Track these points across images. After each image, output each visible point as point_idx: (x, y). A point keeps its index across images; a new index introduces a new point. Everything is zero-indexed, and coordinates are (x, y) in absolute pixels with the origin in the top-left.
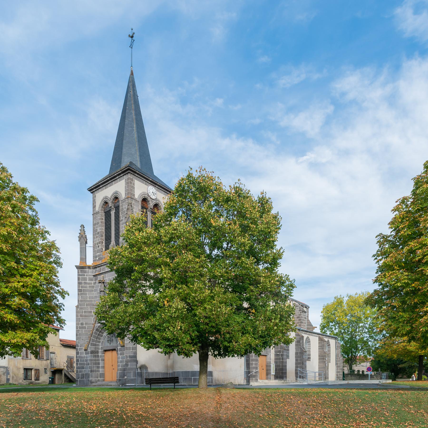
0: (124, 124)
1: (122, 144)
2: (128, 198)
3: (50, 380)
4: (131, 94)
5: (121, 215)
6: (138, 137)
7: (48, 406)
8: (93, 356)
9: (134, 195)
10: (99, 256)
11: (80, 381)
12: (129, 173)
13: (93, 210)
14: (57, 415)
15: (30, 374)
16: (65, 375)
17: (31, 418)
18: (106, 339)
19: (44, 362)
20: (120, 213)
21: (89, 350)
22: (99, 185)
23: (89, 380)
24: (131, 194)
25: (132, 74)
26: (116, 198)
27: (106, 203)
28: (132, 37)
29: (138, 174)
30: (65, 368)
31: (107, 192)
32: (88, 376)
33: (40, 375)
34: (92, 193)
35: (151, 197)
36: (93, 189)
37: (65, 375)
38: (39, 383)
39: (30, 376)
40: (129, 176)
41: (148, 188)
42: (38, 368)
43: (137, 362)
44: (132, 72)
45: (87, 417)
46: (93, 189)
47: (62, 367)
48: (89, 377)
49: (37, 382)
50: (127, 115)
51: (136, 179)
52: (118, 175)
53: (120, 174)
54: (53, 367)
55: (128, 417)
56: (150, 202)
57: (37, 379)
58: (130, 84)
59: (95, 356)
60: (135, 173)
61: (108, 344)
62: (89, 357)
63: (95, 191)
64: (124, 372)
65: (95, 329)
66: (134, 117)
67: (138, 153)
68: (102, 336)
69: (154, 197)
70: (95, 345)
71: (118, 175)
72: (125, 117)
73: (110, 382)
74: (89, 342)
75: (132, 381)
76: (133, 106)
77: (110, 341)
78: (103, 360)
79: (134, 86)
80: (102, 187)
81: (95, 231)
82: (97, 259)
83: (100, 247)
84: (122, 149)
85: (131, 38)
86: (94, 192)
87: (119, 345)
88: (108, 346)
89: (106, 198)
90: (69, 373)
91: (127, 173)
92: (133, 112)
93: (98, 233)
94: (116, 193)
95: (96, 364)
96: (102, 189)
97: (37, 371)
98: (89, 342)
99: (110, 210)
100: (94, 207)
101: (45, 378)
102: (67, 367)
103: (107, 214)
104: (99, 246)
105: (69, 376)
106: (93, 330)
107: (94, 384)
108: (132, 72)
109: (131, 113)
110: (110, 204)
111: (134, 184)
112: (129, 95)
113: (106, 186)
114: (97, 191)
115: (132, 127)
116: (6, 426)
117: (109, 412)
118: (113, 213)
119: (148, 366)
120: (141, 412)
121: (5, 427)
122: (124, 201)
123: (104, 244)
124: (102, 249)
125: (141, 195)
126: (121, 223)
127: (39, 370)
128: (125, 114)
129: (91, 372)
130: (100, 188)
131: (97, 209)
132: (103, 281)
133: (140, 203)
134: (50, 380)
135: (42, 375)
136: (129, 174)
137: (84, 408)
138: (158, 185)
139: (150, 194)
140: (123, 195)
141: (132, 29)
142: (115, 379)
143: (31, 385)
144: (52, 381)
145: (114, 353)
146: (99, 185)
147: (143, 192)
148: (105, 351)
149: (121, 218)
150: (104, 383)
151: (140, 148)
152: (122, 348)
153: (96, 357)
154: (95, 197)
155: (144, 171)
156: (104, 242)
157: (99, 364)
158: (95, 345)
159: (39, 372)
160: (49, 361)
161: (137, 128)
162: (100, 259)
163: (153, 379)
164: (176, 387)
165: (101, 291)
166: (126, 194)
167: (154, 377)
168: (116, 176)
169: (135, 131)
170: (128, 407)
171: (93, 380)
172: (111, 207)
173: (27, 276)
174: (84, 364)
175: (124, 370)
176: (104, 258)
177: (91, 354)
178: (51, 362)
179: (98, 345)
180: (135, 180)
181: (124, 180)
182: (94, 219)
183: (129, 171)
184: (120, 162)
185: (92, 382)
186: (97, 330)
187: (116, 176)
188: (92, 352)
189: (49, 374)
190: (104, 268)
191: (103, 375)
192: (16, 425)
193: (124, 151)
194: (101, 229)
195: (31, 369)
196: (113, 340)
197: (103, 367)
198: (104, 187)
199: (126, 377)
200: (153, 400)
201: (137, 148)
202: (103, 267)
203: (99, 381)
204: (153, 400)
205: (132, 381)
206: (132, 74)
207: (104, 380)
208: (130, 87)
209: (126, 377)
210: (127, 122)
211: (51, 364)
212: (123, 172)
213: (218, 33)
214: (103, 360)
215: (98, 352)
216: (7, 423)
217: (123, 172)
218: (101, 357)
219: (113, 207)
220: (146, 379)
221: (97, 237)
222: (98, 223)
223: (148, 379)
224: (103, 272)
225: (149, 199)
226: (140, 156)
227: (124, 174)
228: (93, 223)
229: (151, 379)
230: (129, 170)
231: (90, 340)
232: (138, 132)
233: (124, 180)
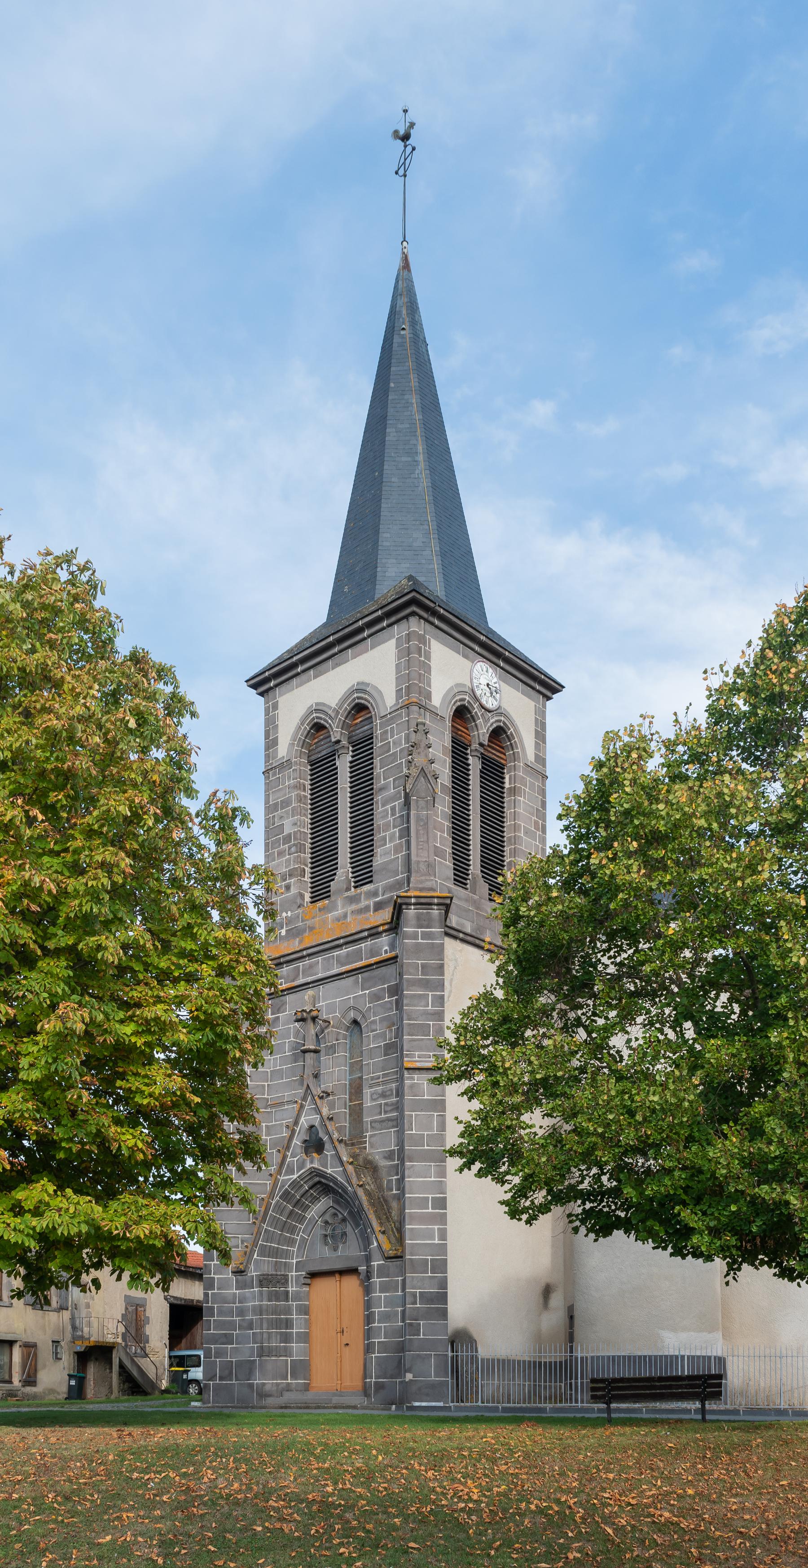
0: (383, 442)
1: (377, 514)
2: (407, 706)
3: (73, 1383)
4: (403, 337)
5: (378, 770)
6: (434, 486)
7: (289, 1480)
8: (270, 1293)
9: (429, 696)
10: (289, 921)
11: (217, 1388)
12: (413, 614)
13: (267, 757)
14: (340, 1517)
15: (6, 1359)
16: (122, 1366)
17: (245, 1529)
18: (318, 1231)
19: (53, 1317)
20: (377, 761)
21: (253, 1272)
22: (294, 666)
23: (251, 1386)
24: (420, 693)
25: (406, 265)
26: (360, 708)
27: (318, 727)
28: (406, 138)
29: (442, 618)
30: (119, 1340)
31: (326, 689)
32: (247, 1368)
33: (39, 1366)
34: (261, 694)
35: (484, 702)
36: (267, 680)
37: (122, 1366)
38: (35, 1397)
39: (6, 1368)
40: (415, 626)
41: (471, 671)
42: (31, 1340)
43: (443, 1314)
44: (405, 259)
45: (462, 1527)
46: (267, 680)
47: (110, 1339)
48: (250, 1374)
49: (29, 1390)
50: (391, 411)
51: (436, 638)
53: (379, 620)
54: (82, 1338)
55: (618, 1530)
57: (30, 1380)
58: (400, 302)
59: (276, 1296)
60: (434, 613)
61: (327, 1252)
62: (254, 1297)
63: (276, 686)
64: (399, 1355)
65: (278, 1193)
66: (418, 417)
67: (434, 545)
68: (301, 1219)
69: (490, 703)
70: (275, 1253)
72: (384, 418)
73: (334, 1395)
74: (255, 1243)
75: (433, 1392)
76: (413, 377)
77: (334, 1238)
78: (305, 1310)
79: (413, 308)
81: (272, 830)
82: (283, 932)
83: (294, 891)
84: (377, 532)
86: (271, 688)
87: (376, 1254)
88: (327, 1256)
90: (133, 1361)
91: (406, 617)
92: (414, 400)
93: (287, 839)
94: (361, 688)
95: (277, 1324)
96: (303, 677)
97: (30, 1347)
98: (255, 1243)
99: (332, 755)
100: (271, 743)
101: (54, 1377)
102: (124, 1336)
103: (322, 771)
104: (288, 888)
105: (135, 1373)
106: (272, 1195)
107: (270, 1401)
108: (405, 259)
110: (336, 733)
111: (428, 656)
112: (396, 339)
114: (284, 687)
115: (413, 453)
116: (166, 1556)
117: (541, 1511)
118: (344, 764)
119: (476, 1336)
120: (667, 1514)
121: (160, 1561)
122: (391, 718)
123: (307, 878)
124: (302, 896)
126: (379, 798)
127: (34, 1346)
128: (385, 406)
129: (260, 1355)
130: (298, 674)
131: (283, 750)
132: (314, 1014)
133: (448, 723)
134: (73, 1383)
135: (44, 1366)
136: (413, 620)
137: (433, 1490)
139: (478, 693)
140: (388, 696)
141: (405, 111)
142: (352, 1379)
143: (12, 1401)
144: (77, 1392)
145: (351, 1284)
146: (294, 666)
147: (457, 685)
148: (313, 1275)
150: (309, 1396)
152: (393, 1265)
153: (277, 1300)
154: (275, 707)
155: (458, 606)
156: (308, 870)
157: (288, 1324)
158: (275, 1253)
159: (35, 1355)
160: (66, 1315)
161: (429, 455)
162: (293, 933)
163: (622, 1380)
164: (708, 1417)
165: (304, 1052)
166: (399, 691)
167: (645, 1373)
168: (360, 630)
169: (422, 465)
170: (604, 1490)
171: (267, 1388)
172: (338, 742)
173: (176, 981)
174: (232, 1325)
175: (401, 1348)
176: (311, 929)
177: (261, 1285)
178: (73, 1319)
179: (287, 1254)
180: (434, 643)
181: (393, 642)
182: (268, 787)
184: (373, 580)
185: (263, 1394)
186: (286, 1196)
187: (360, 630)
188: (264, 1281)
189: (67, 1362)
190: (311, 966)
191: (301, 1368)
192: (198, 1555)
193: (387, 538)
194: (298, 823)
195: (11, 1343)
196: (344, 1234)
197: (305, 1338)
198: (312, 672)
199: (409, 1376)
200: (694, 1465)
201: (432, 526)
202: (307, 962)
203: (288, 1388)
204: (694, 1465)
205: (433, 1392)
206: (406, 265)
207: (307, 1388)
209: (409, 1376)
210: (391, 435)
211: (74, 1328)
212: (388, 615)
214: (305, 1310)
215: (284, 1281)
216: (162, 1544)
217: (388, 615)
218: (297, 1297)
219: (344, 742)
220: (593, 1381)
221: (281, 854)
222: (286, 803)
223: (602, 1381)
224: (309, 979)
225: (476, 709)
226: (443, 555)
227: (393, 619)
228: (267, 801)
229: (615, 1380)
230: (413, 604)
231: (259, 1233)
232: (432, 469)
233: (393, 642)
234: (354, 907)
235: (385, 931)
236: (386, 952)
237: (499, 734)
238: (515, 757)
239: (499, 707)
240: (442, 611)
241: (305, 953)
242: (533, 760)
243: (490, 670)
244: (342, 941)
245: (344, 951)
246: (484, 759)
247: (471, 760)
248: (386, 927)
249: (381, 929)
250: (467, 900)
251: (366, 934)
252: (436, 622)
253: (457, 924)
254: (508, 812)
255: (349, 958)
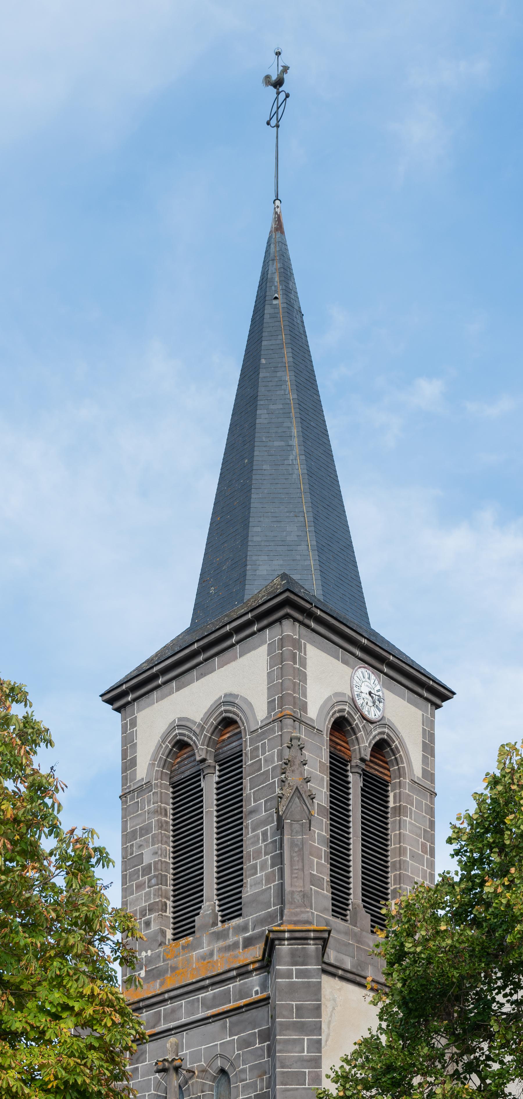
0: (253, 425)
1: (246, 506)
2: (280, 719)
4: (276, 307)
5: (248, 791)
6: (310, 473)
9: (304, 707)
13: (124, 780)
20: (246, 782)
22: (154, 677)
24: (294, 704)
25: (279, 226)
26: (228, 723)
27: (181, 745)
28: (278, 84)
31: (191, 702)
34: (118, 710)
35: (365, 712)
36: (124, 694)
40: (289, 629)
41: (352, 678)
44: (278, 220)
46: (124, 694)
51: (313, 643)
52: (238, 630)
53: (249, 624)
56: (361, 734)
58: (272, 269)
60: (310, 615)
63: (134, 700)
67: (311, 540)
69: (373, 714)
71: (238, 630)
79: (287, 274)
80: (165, 683)
83: (154, 927)
84: (246, 526)
85: (272, 91)
86: (129, 703)
89: (182, 724)
91: (279, 620)
92: (288, 377)
93: (147, 870)
94: (229, 700)
96: (165, 689)
99: (197, 776)
100: (129, 764)
103: (185, 794)
104: (148, 924)
108: (278, 220)
109: (281, 382)
110: (202, 750)
112: (268, 310)
113: (183, 679)
118: (210, 786)
123: (169, 913)
124: (163, 933)
125: (328, 704)
126: (249, 822)
128: (255, 386)
130: (159, 686)
132: (177, 1063)
133: (326, 737)
138: (391, 665)
139: (359, 702)
140: (258, 708)
141: (278, 54)
146: (154, 677)
147: (336, 694)
149: (250, 803)
151: (316, 518)
154: (134, 723)
156: (170, 904)
161: (305, 438)
169: (296, 450)
172: (203, 761)
176: (174, 969)
181: (264, 648)
183: (288, 610)
184: (242, 579)
190: (173, 1011)
193: (258, 531)
194: (159, 852)
198: (174, 684)
201: (308, 518)
202: (169, 1006)
206: (279, 226)
208: (272, 280)
210: (262, 417)
213: (422, 134)
217: (259, 618)
219: (210, 761)
221: (140, 886)
222: (145, 830)
224: (172, 1025)
225: (357, 721)
226: (320, 550)
227: (265, 622)
228: (124, 829)
230: (287, 605)
232: (308, 454)
233: (264, 648)
234: (221, 944)
235: (255, 970)
236: (257, 993)
237: (382, 748)
238: (400, 773)
239: (383, 718)
240: (319, 612)
241: (166, 996)
242: (420, 776)
243: (373, 677)
244: (207, 982)
245: (210, 993)
246: (366, 775)
247: (351, 778)
248: (257, 965)
249: (251, 967)
250: (346, 933)
251: (234, 973)
252: (313, 625)
253: (336, 959)
254: (392, 834)
255: (216, 1001)
